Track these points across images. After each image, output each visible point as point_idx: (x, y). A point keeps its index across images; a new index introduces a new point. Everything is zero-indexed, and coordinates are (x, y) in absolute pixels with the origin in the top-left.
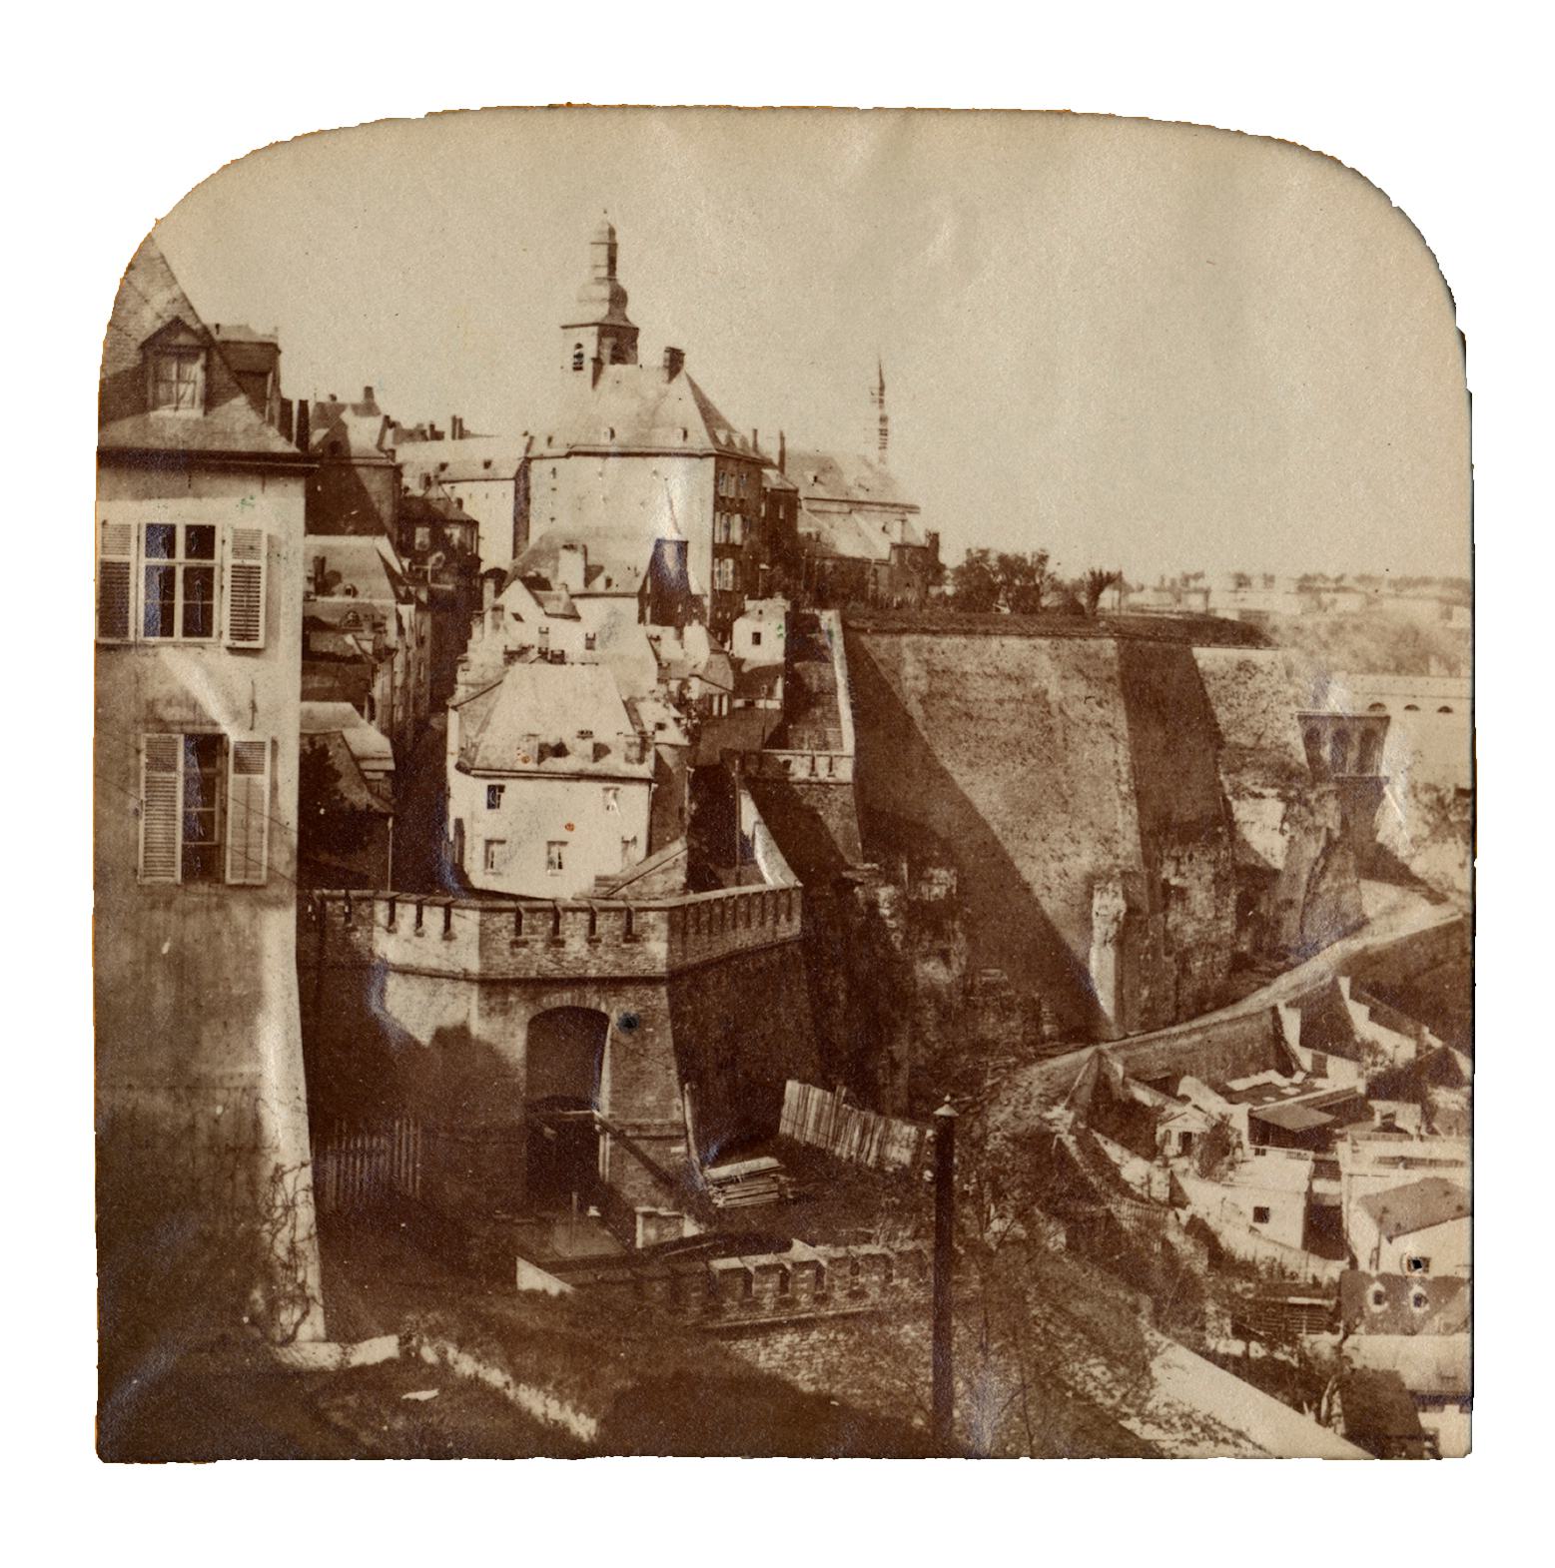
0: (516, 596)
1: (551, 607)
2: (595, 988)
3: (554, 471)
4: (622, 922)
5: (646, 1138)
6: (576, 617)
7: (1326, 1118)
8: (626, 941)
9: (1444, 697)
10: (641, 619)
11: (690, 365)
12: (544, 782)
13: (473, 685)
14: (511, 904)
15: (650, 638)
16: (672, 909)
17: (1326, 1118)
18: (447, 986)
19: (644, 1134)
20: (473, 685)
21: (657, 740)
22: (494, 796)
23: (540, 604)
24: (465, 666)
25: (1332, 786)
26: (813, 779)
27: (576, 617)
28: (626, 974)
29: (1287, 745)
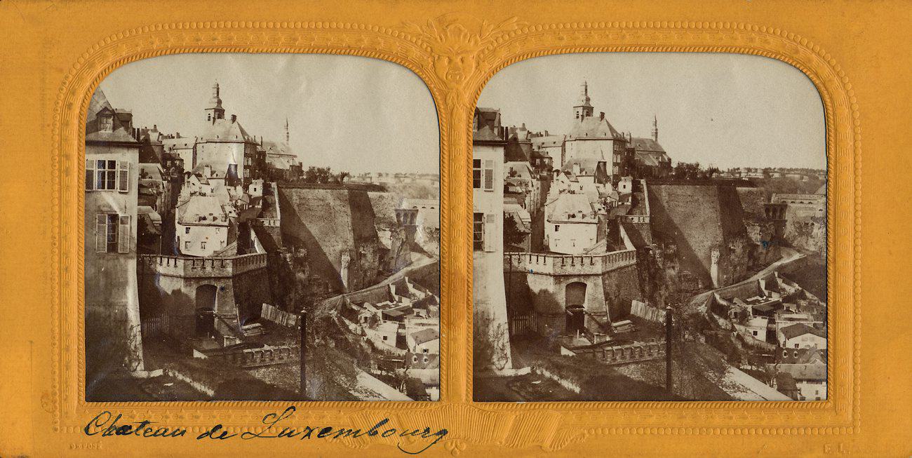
0: (193, 179)
4: (220, 263)
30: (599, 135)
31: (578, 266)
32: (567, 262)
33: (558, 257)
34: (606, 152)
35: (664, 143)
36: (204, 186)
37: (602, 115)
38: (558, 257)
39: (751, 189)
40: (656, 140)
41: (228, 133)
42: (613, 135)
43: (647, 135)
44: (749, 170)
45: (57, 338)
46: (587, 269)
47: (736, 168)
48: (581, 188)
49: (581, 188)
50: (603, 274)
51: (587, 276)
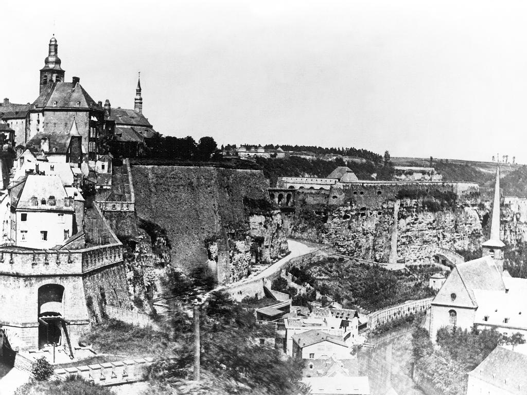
0: (27, 155)
1: (39, 157)
2: (59, 277)
3: (28, 161)
4: (67, 257)
5: (77, 325)
6: (47, 161)
7: (281, 312)
8: (69, 263)
9: (519, 329)
10: (67, 162)
11: (81, 83)
12: (39, 213)
13: (16, 182)
14: (32, 252)
15: (71, 167)
16: (83, 253)
17: (281, 312)
18: (12, 278)
19: (76, 323)
20: (16, 182)
21: (75, 199)
22: (24, 218)
23: (35, 157)
24: (12, 176)
25: (279, 211)
26: (122, 210)
27: (47, 161)
28: (69, 333)
29: (413, 335)
30: (73, 104)
31: (52, 263)
32: (39, 260)
33: (28, 254)
34: (79, 126)
35: (148, 112)
36: (41, 164)
37: (76, 80)
38: (28, 254)
39: (254, 171)
40: (141, 112)
41: (67, 100)
42: (89, 105)
43: (128, 105)
44: (248, 148)
45: (122, 356)
46: (65, 268)
47: (231, 145)
48: (52, 168)
49: (52, 168)
50: (84, 276)
51: (66, 276)
